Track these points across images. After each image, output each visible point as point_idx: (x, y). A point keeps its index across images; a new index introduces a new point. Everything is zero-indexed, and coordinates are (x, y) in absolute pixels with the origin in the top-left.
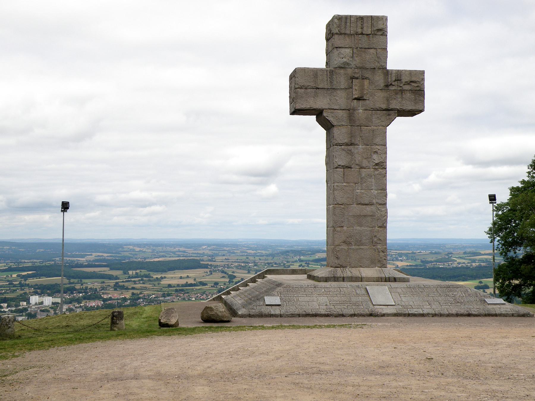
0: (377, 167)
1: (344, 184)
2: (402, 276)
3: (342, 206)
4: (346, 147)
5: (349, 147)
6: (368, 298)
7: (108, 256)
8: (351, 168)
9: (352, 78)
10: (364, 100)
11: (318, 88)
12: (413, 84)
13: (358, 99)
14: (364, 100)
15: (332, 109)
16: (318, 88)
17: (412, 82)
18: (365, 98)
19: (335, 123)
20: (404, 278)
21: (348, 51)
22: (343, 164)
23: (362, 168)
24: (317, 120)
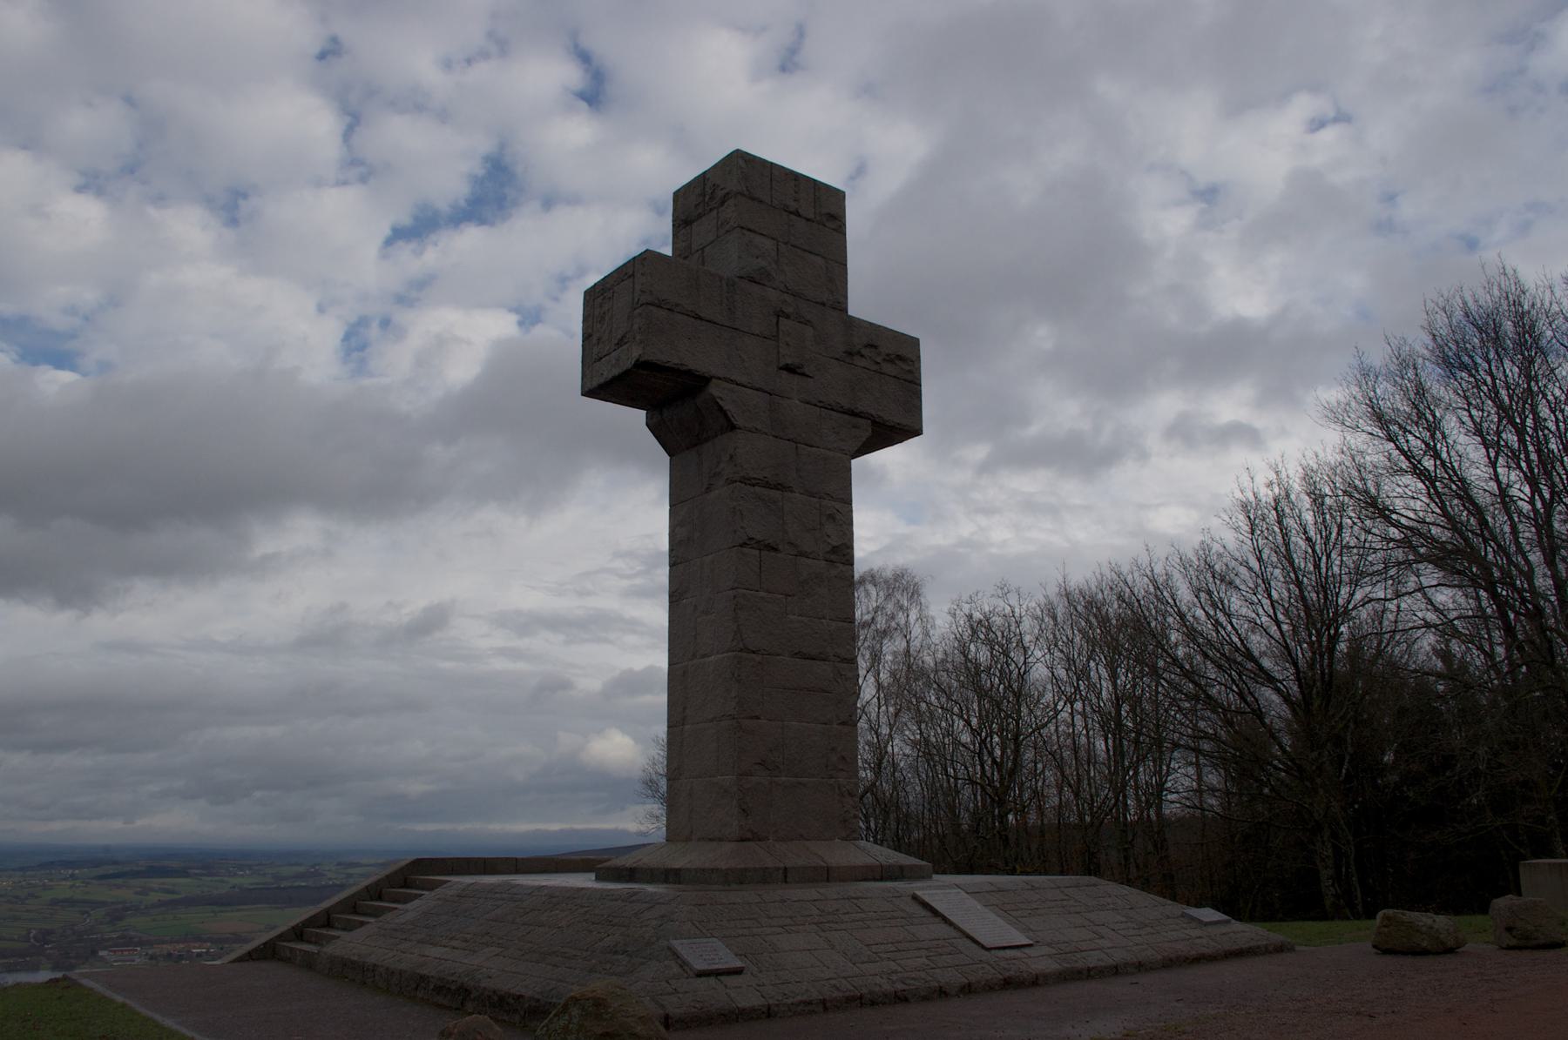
0: (833, 557)
1: (762, 594)
2: (312, 913)
3: (758, 658)
4: (765, 491)
5: (775, 494)
6: (941, 930)
7: (502, 652)
8: (775, 550)
9: (780, 314)
10: (803, 374)
11: (700, 318)
12: (900, 363)
13: (790, 369)
14: (803, 374)
15: (732, 381)
16: (700, 318)
17: (900, 358)
18: (806, 370)
19: (739, 421)
20: (901, 868)
21: (768, 244)
22: (759, 537)
23: (802, 554)
24: (650, 425)
